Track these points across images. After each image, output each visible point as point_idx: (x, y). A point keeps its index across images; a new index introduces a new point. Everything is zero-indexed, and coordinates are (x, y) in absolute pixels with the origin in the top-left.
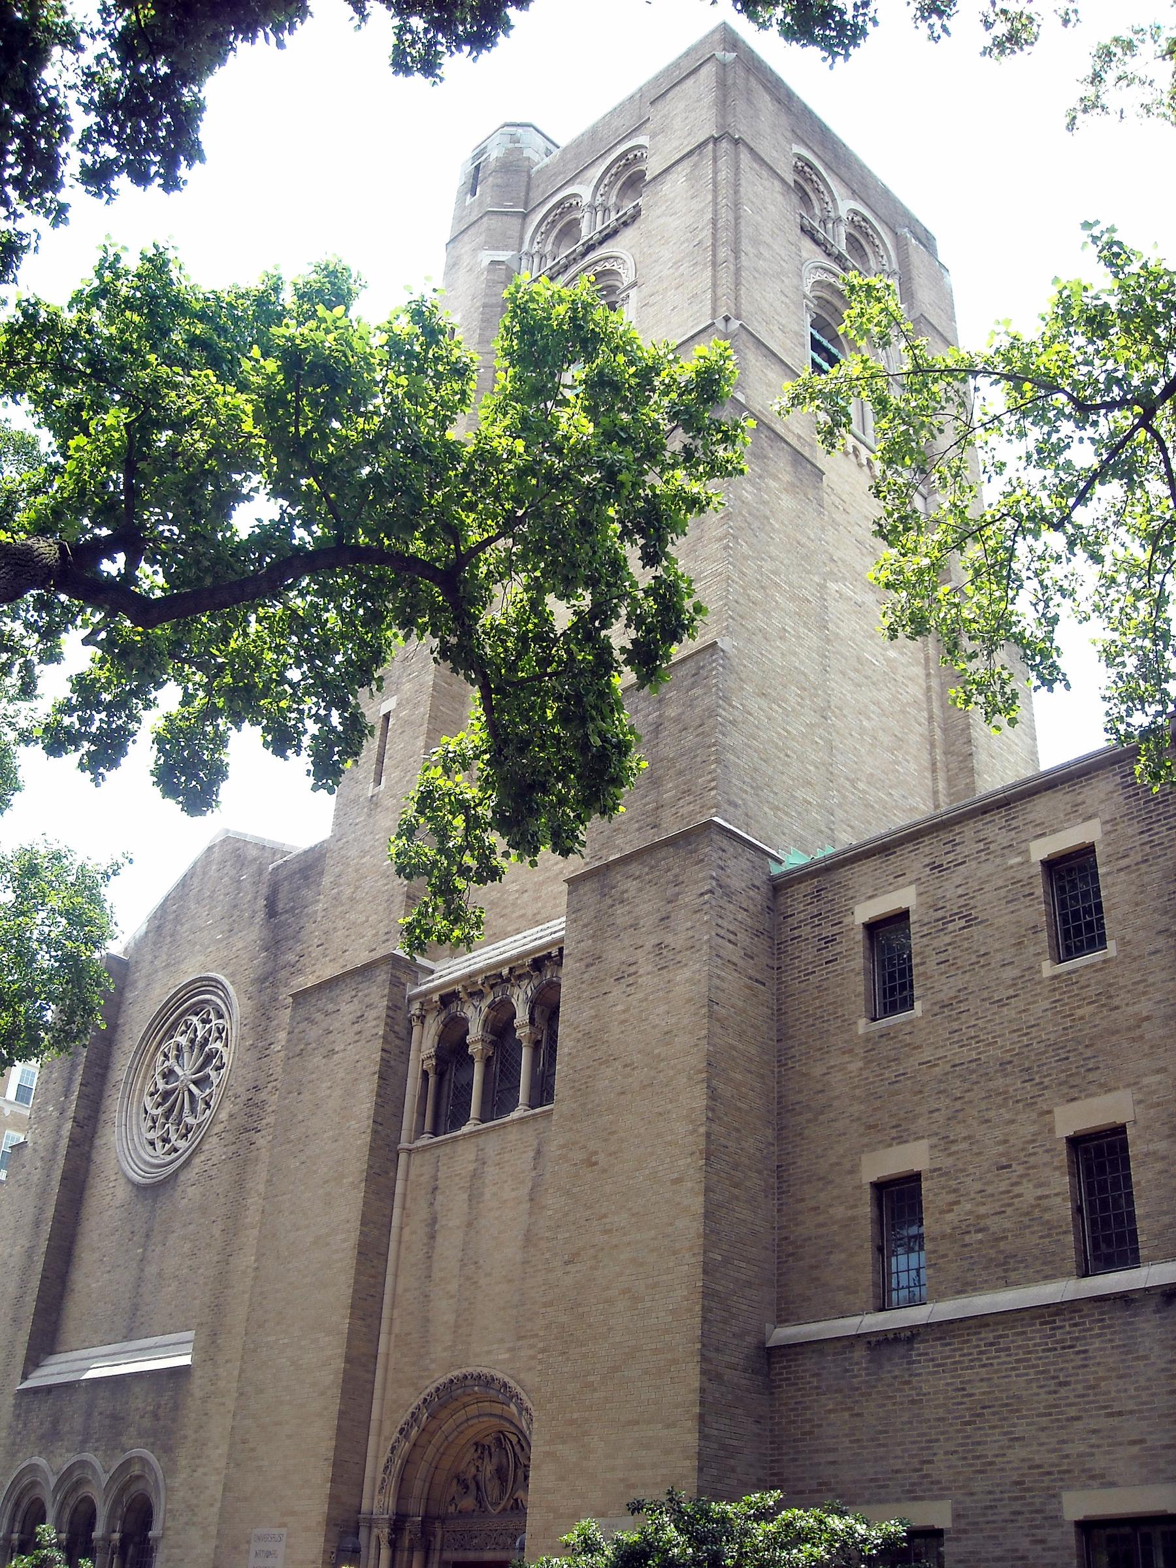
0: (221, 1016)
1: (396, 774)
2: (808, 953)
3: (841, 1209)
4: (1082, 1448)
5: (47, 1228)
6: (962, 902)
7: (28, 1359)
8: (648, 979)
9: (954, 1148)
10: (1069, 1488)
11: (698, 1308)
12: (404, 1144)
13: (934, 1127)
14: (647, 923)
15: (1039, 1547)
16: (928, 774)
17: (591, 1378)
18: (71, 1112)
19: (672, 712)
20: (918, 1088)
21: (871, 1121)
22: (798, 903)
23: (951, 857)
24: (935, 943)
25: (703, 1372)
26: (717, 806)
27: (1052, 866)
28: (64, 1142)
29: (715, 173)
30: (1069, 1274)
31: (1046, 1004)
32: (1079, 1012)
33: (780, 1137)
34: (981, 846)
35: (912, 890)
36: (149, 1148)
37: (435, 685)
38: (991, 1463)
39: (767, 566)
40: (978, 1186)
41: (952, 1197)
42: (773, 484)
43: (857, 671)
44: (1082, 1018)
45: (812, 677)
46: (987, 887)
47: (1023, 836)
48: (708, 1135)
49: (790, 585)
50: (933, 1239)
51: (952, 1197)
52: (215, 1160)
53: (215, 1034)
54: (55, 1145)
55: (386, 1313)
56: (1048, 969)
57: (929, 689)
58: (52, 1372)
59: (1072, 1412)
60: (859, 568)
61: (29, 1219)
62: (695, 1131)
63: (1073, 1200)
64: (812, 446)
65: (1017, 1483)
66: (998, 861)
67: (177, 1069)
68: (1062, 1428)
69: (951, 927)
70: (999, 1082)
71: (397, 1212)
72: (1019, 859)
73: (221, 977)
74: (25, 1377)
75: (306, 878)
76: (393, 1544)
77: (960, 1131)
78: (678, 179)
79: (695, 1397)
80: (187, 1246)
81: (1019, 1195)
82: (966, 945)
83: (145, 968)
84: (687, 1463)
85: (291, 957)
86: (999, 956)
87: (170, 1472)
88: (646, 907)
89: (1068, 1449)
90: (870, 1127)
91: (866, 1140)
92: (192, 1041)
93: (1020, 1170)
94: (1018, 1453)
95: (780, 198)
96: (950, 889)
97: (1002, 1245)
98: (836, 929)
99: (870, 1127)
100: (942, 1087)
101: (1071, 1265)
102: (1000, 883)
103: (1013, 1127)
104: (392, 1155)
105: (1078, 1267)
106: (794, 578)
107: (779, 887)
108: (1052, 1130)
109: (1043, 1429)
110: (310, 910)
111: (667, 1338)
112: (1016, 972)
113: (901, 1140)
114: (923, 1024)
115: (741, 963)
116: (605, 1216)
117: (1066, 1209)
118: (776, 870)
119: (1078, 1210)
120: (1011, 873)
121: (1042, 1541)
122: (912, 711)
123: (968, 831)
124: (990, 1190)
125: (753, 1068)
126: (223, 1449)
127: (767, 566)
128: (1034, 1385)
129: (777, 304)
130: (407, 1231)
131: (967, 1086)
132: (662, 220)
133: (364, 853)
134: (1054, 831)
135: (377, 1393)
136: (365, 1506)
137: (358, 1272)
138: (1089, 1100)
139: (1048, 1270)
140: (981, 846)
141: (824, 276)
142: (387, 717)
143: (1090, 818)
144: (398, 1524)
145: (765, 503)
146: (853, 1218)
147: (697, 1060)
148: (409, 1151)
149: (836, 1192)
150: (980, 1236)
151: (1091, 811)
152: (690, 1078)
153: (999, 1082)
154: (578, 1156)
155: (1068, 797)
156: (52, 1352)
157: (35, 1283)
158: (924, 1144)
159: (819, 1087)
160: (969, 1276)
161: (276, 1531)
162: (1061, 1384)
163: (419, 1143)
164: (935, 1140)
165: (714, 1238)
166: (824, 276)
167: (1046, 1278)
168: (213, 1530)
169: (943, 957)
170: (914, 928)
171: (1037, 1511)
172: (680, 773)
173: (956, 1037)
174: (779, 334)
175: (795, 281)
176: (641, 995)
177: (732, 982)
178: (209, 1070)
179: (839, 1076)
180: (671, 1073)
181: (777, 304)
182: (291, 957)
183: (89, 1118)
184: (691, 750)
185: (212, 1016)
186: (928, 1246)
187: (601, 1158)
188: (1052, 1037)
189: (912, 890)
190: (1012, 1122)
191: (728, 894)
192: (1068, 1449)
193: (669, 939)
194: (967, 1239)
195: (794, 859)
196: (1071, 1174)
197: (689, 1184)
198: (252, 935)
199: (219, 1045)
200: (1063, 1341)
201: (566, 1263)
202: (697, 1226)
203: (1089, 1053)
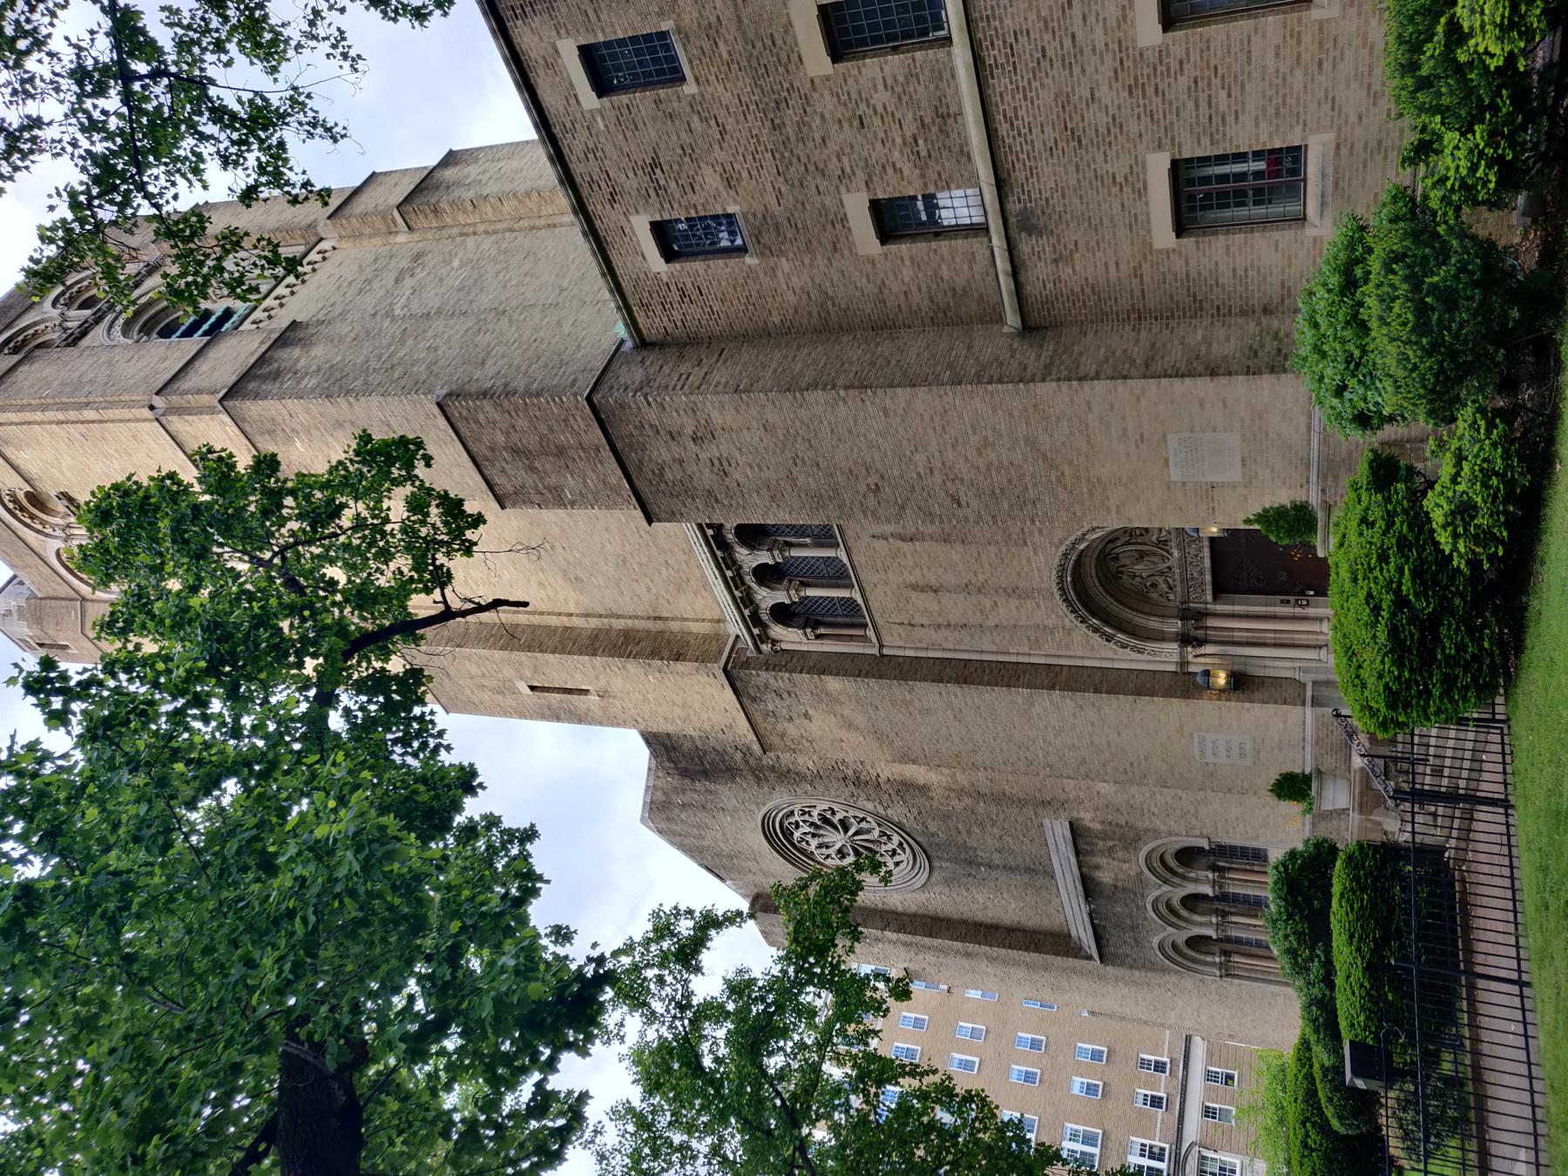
0: (792, 813)
1: (579, 677)
2: (695, 312)
3: (904, 271)
4: (1099, 30)
5: (971, 947)
6: (640, 172)
7: (1076, 956)
8: (721, 448)
9: (848, 170)
10: (1134, 40)
11: (989, 387)
12: (875, 651)
13: (832, 189)
14: (677, 451)
15: (1186, 66)
16: (557, 230)
17: (1053, 478)
18: (878, 933)
19: (501, 439)
20: (799, 206)
21: (830, 248)
22: (652, 325)
23: (603, 184)
24: (677, 196)
25: (1043, 380)
26: (575, 395)
27: (602, 87)
28: (902, 936)
29: (11, 424)
30: (949, 54)
31: (720, 88)
32: (725, 55)
33: (848, 329)
34: (591, 156)
35: (634, 219)
36: (902, 866)
37: (501, 649)
38: (1114, 118)
39: (373, 364)
40: (879, 146)
41: (890, 171)
42: (302, 363)
43: (469, 292)
44: (730, 53)
45: (470, 324)
46: (626, 149)
47: (579, 116)
48: (846, 388)
49: (390, 345)
50: (926, 185)
51: (890, 171)
52: (906, 811)
53: (806, 817)
54: (906, 944)
55: (1013, 659)
56: (690, 88)
57: (486, 232)
58: (1083, 934)
59: (1068, 43)
60: (382, 292)
61: (964, 962)
62: (844, 400)
63: (887, 54)
64: (271, 332)
65: (1131, 93)
66: (602, 140)
67: (837, 846)
68: (1082, 51)
69: (662, 182)
70: (790, 130)
71: (931, 654)
72: (599, 119)
73: (760, 816)
74: (1090, 958)
75: (674, 749)
76: (1201, 642)
77: (833, 164)
78: (22, 458)
79: (1064, 385)
80: (976, 830)
81: (885, 108)
82: (676, 167)
83: (760, 879)
84: (1120, 389)
85: (738, 756)
86: (683, 135)
87: (1156, 833)
88: (664, 452)
89: (1100, 45)
90: (835, 248)
91: (846, 253)
92: (814, 835)
93: (863, 106)
94: (1104, 93)
95: (36, 366)
96: (631, 183)
97: (927, 120)
98: (673, 288)
99: (835, 248)
100: (797, 183)
101: (941, 53)
102: (621, 137)
103: (827, 116)
104: (886, 660)
105: (943, 46)
106: (384, 343)
107: (643, 344)
108: (828, 78)
109: (1083, 70)
110: (699, 744)
111: (1016, 413)
112: (696, 119)
113: (844, 220)
114: (745, 205)
115: (705, 369)
116: (919, 474)
117: (894, 60)
118: (629, 344)
119: (895, 50)
120: (612, 128)
121: (1181, 63)
122: (504, 245)
123: (578, 169)
124: (881, 135)
125: (791, 355)
126: (1134, 790)
127: (373, 364)
128: (1045, 81)
129: (139, 365)
130: (945, 645)
131: (795, 161)
132: (67, 473)
133: (645, 700)
134: (572, 86)
135: (1079, 663)
136: (1172, 668)
137: (981, 683)
138: (800, 42)
139: (946, 76)
140: (591, 156)
141: (117, 328)
142: (532, 688)
143: (557, 51)
144: (1185, 640)
145: (318, 370)
146: (912, 259)
147: (786, 400)
148: (881, 646)
149: (891, 277)
150: (921, 142)
151: (550, 50)
152: (801, 406)
153: (790, 130)
154: (871, 501)
155: (541, 73)
156: (1069, 936)
157: (1014, 954)
158: (846, 198)
159: (804, 296)
160: (956, 149)
161: (1196, 741)
162: (1044, 56)
163: (874, 639)
164: (842, 189)
165: (931, 378)
166: (117, 328)
167: (953, 77)
168: (1201, 795)
169: (688, 188)
170: (666, 217)
171: (1155, 70)
172: (551, 429)
173: (754, 173)
174: (168, 363)
175: (117, 350)
176: (737, 453)
177: (720, 375)
178: (835, 820)
179: (794, 279)
180: (798, 423)
181: (139, 365)
182: (738, 756)
183: (882, 918)
184: (531, 421)
185: (792, 820)
186: (931, 190)
187: (872, 480)
188: (748, 81)
189: (634, 219)
190: (822, 116)
191: (648, 381)
192: (1100, 45)
193: (689, 431)
194: (924, 153)
195: (621, 331)
196: (864, 58)
197: (888, 401)
198: (726, 793)
199: (815, 813)
200: (1006, 56)
201: (960, 505)
202: (922, 392)
203: (759, 45)
